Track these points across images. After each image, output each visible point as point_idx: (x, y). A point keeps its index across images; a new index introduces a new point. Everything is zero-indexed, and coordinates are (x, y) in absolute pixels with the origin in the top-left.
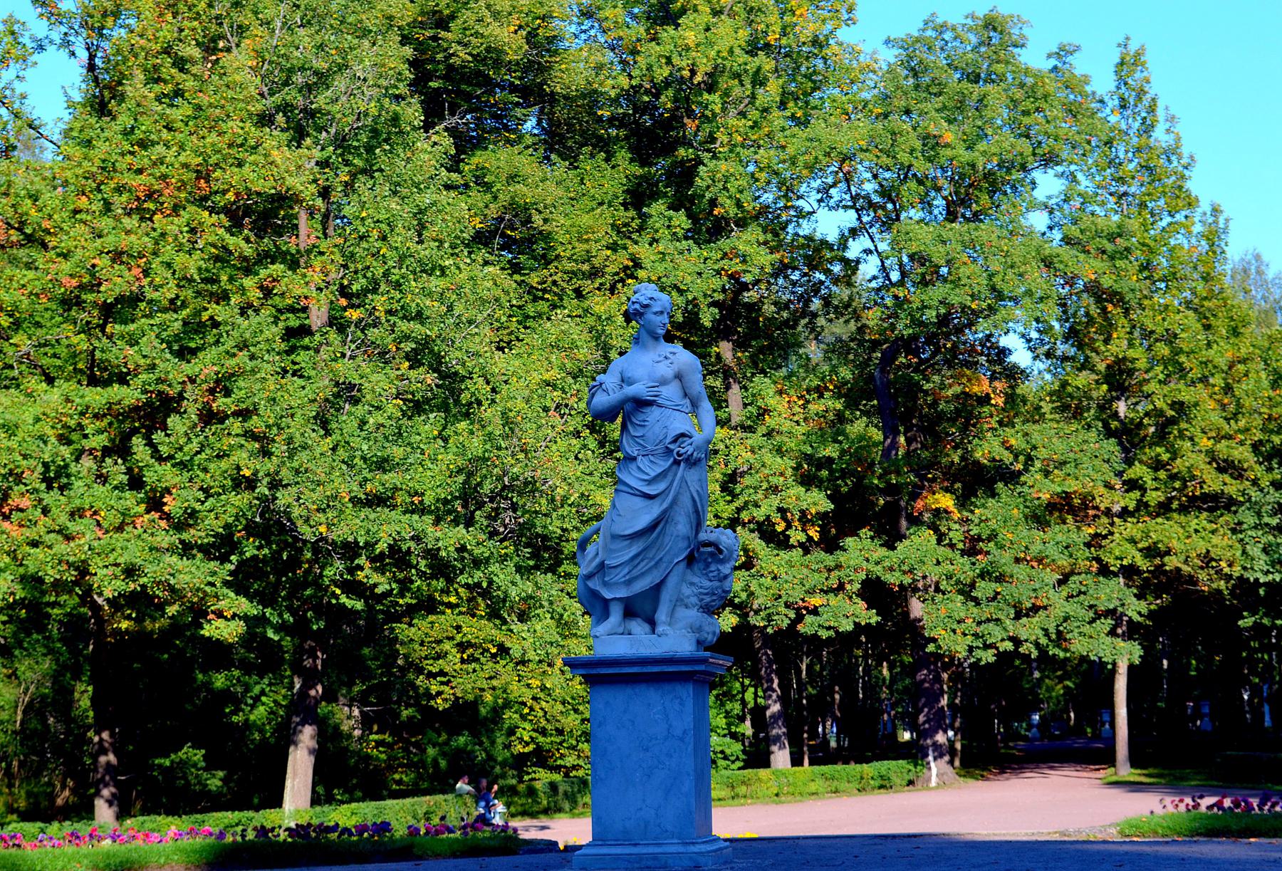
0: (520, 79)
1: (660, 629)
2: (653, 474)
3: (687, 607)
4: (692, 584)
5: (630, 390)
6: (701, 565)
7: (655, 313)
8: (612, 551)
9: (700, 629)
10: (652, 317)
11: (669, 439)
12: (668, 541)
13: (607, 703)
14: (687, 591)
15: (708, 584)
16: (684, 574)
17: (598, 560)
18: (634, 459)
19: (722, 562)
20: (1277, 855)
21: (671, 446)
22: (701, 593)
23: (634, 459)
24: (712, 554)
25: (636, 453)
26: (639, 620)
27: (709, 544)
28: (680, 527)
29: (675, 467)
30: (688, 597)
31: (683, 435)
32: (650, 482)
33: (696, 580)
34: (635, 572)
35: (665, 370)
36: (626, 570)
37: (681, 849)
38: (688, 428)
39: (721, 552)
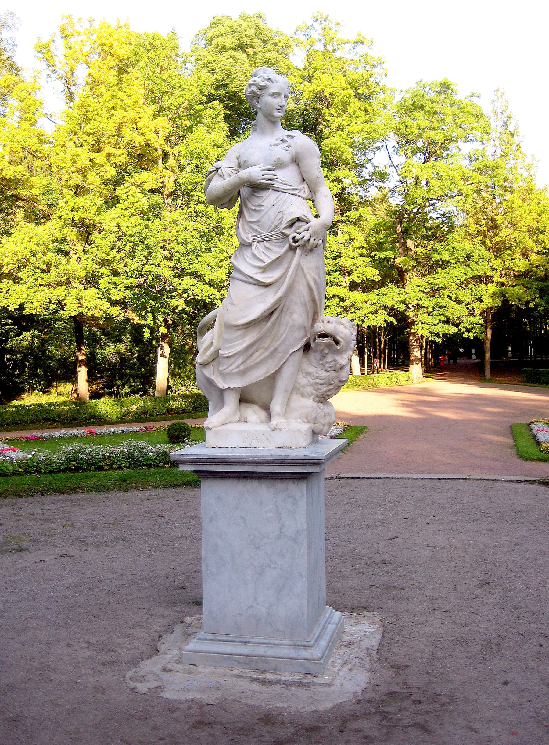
1: (275, 422)
2: (268, 261)
3: (303, 395)
4: (308, 374)
5: (244, 173)
6: (318, 355)
7: (273, 95)
8: (227, 341)
9: (315, 420)
10: (270, 99)
11: (284, 225)
12: (283, 332)
13: (218, 498)
14: (303, 381)
15: (324, 374)
16: (300, 364)
17: (212, 349)
18: (250, 245)
19: (338, 352)
21: (287, 232)
22: (317, 384)
23: (250, 245)
24: (328, 346)
25: (250, 240)
26: (255, 407)
27: (324, 336)
28: (296, 316)
29: (291, 253)
30: (304, 386)
31: (299, 220)
32: (265, 269)
33: (312, 370)
34: (250, 363)
35: (283, 153)
36: (240, 361)
37: (292, 653)
38: (305, 213)
39: (337, 342)
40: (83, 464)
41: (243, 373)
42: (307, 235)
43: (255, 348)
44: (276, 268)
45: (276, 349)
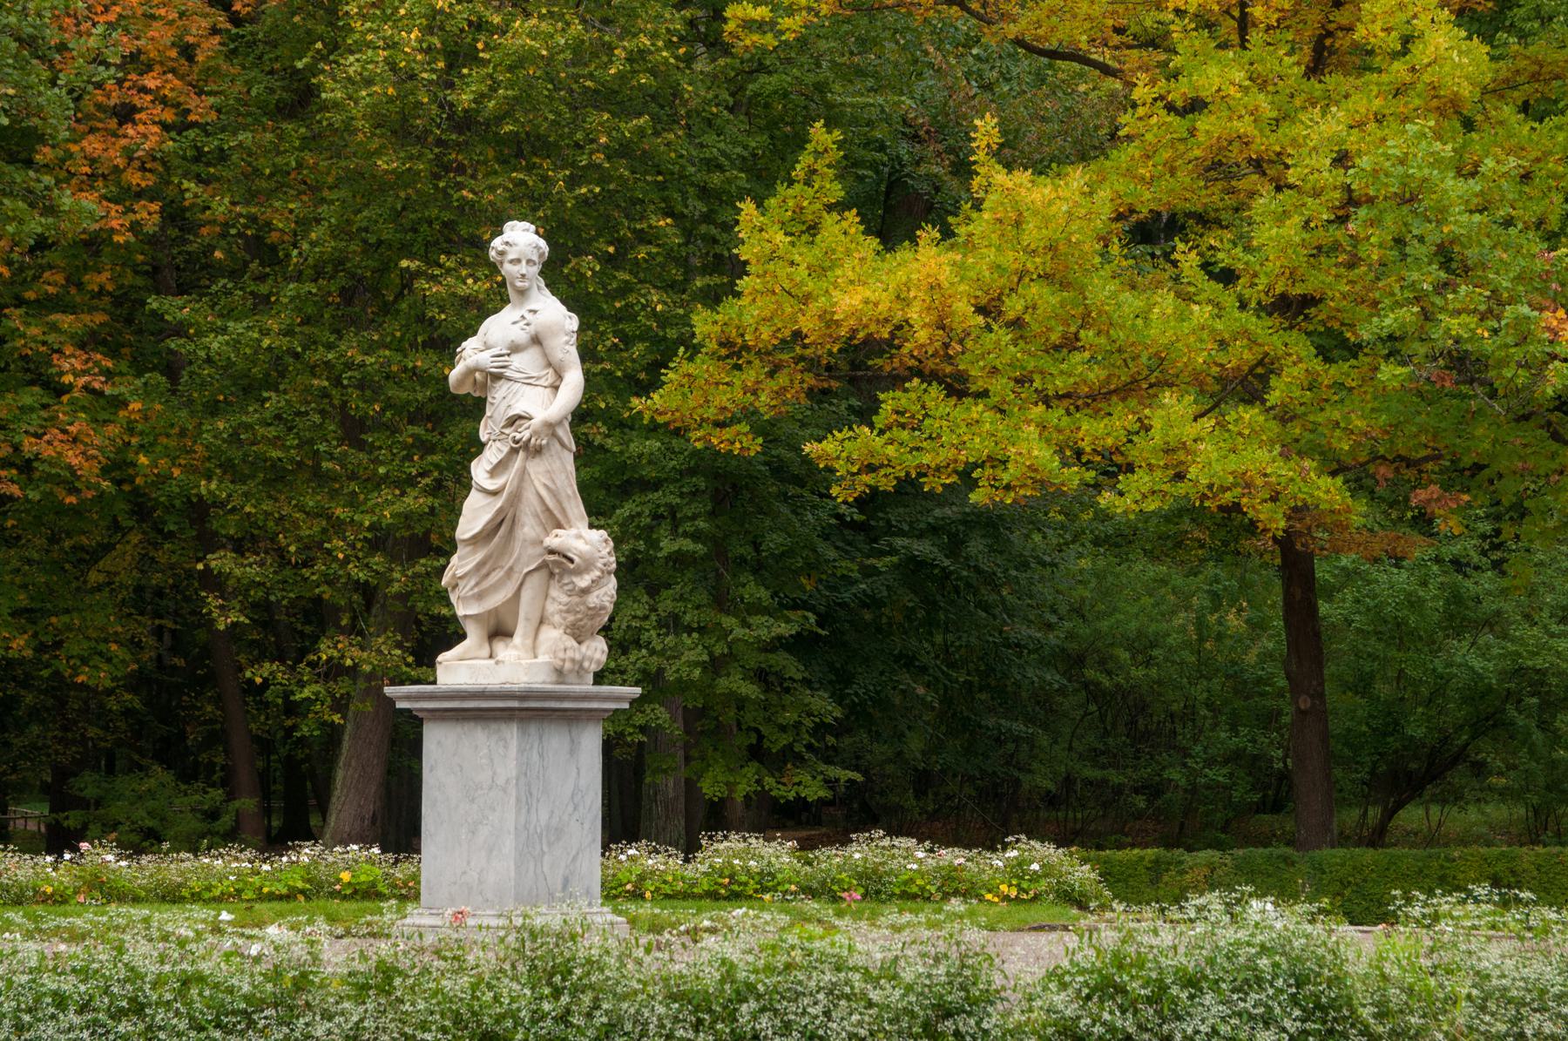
0: (319, 122)
7: (511, 262)
20: (3, 473)
31: (520, 417)
36: (473, 582)
40: (746, 884)
41: (480, 597)
42: (526, 435)
43: (488, 567)
44: (502, 473)
45: (511, 569)
